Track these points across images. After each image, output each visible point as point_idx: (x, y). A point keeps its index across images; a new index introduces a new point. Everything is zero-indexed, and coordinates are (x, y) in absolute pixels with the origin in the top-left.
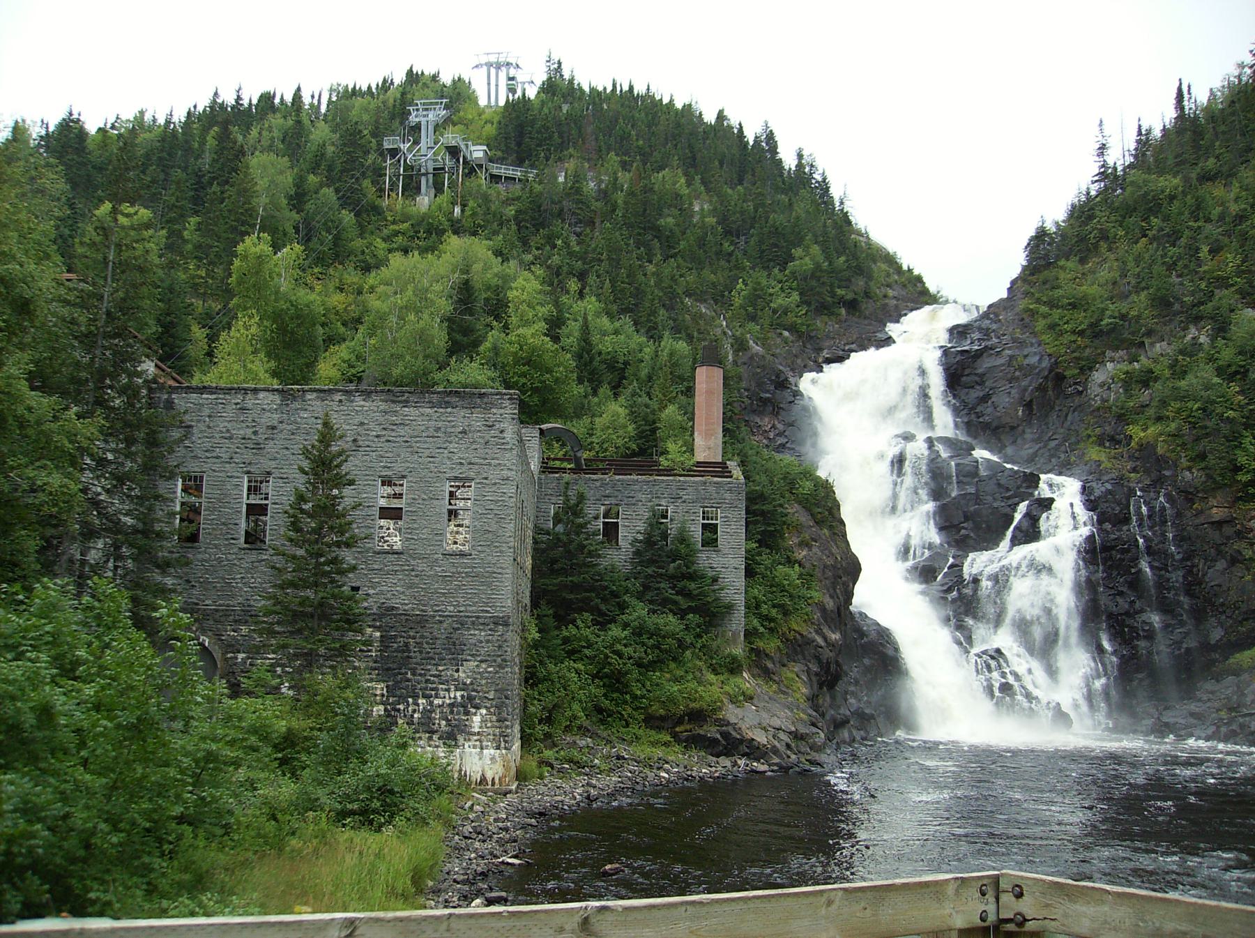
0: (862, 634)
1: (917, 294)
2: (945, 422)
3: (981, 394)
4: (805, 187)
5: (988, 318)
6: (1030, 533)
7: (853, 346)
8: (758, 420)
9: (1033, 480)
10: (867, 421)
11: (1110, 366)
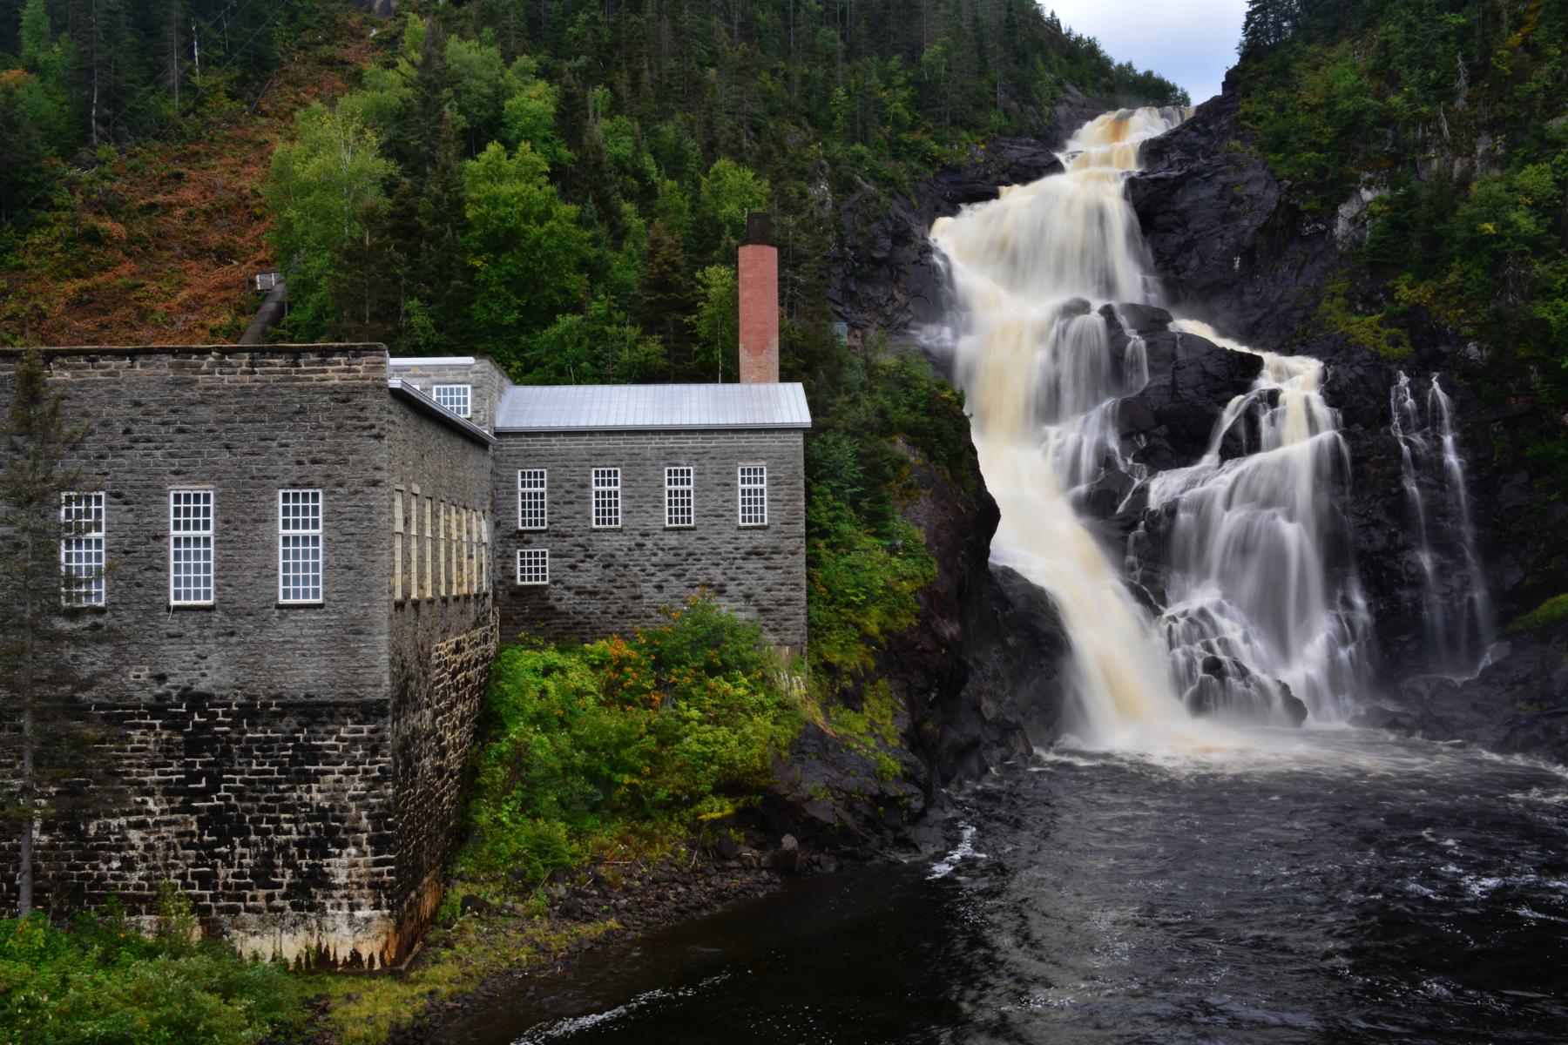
0: (1006, 602)
2: (1134, 285)
3: (1182, 240)
5: (1195, 129)
6: (1244, 442)
8: (870, 290)
9: (1253, 367)
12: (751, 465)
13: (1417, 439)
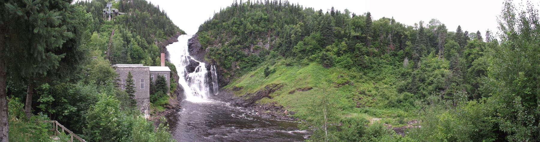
1: (184, 33)
2: (187, 54)
4: (163, 14)
10: (178, 52)
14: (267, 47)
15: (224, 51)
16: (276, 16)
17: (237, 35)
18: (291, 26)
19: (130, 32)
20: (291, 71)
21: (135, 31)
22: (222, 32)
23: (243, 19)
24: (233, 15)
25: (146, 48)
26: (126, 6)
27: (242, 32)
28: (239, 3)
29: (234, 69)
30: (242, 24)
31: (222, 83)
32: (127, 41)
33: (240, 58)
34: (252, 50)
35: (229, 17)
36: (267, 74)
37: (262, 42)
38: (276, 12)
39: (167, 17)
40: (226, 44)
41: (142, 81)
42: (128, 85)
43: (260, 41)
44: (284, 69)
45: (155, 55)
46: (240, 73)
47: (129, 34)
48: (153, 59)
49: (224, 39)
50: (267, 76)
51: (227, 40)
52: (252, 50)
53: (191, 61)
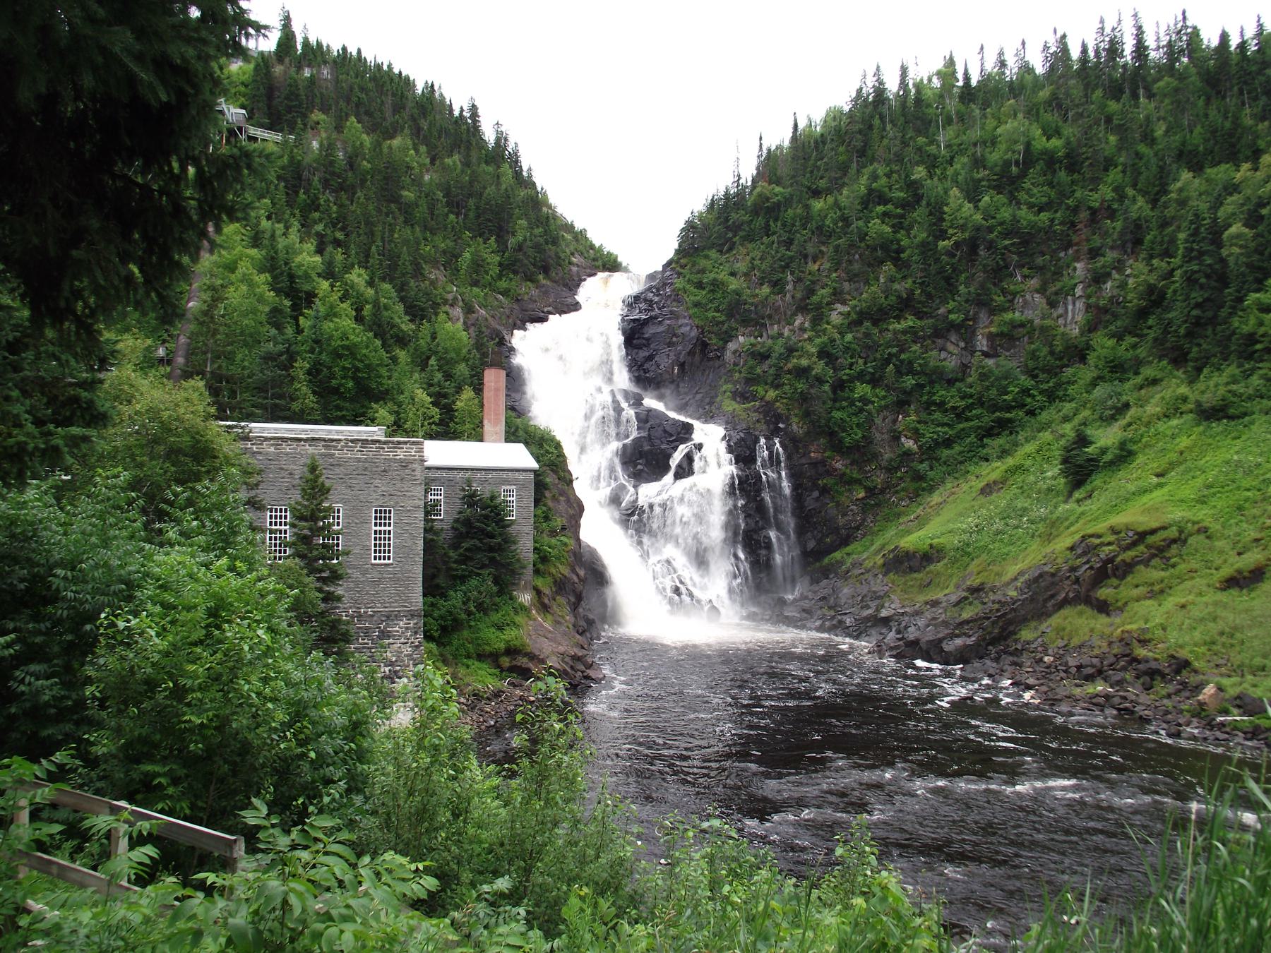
2: (623, 378)
4: (500, 156)
6: (685, 470)
7: (550, 309)
10: (570, 367)
11: (741, 339)
12: (508, 487)
13: (770, 474)
14: (1072, 319)
15: (823, 354)
16: (1121, 130)
17: (896, 260)
18: (1220, 173)
19: (310, 246)
20: (1227, 451)
21: (337, 243)
22: (811, 249)
23: (919, 172)
24: (863, 154)
25: (402, 341)
26: (293, 94)
27: (924, 244)
28: (892, 86)
29: (888, 455)
30: (918, 198)
31: (822, 543)
32: (295, 293)
33: (916, 390)
34: (982, 343)
35: (844, 168)
36: (1081, 470)
37: (1042, 290)
38: (1113, 106)
39: (518, 174)
40: (836, 316)
41: (383, 519)
42: (305, 540)
43: (1026, 286)
44: (1184, 442)
45: (448, 376)
46: (919, 477)
47: (307, 258)
48: (439, 399)
49: (823, 293)
50: (1078, 484)
51: (838, 296)
52: (982, 343)
53: (646, 418)
